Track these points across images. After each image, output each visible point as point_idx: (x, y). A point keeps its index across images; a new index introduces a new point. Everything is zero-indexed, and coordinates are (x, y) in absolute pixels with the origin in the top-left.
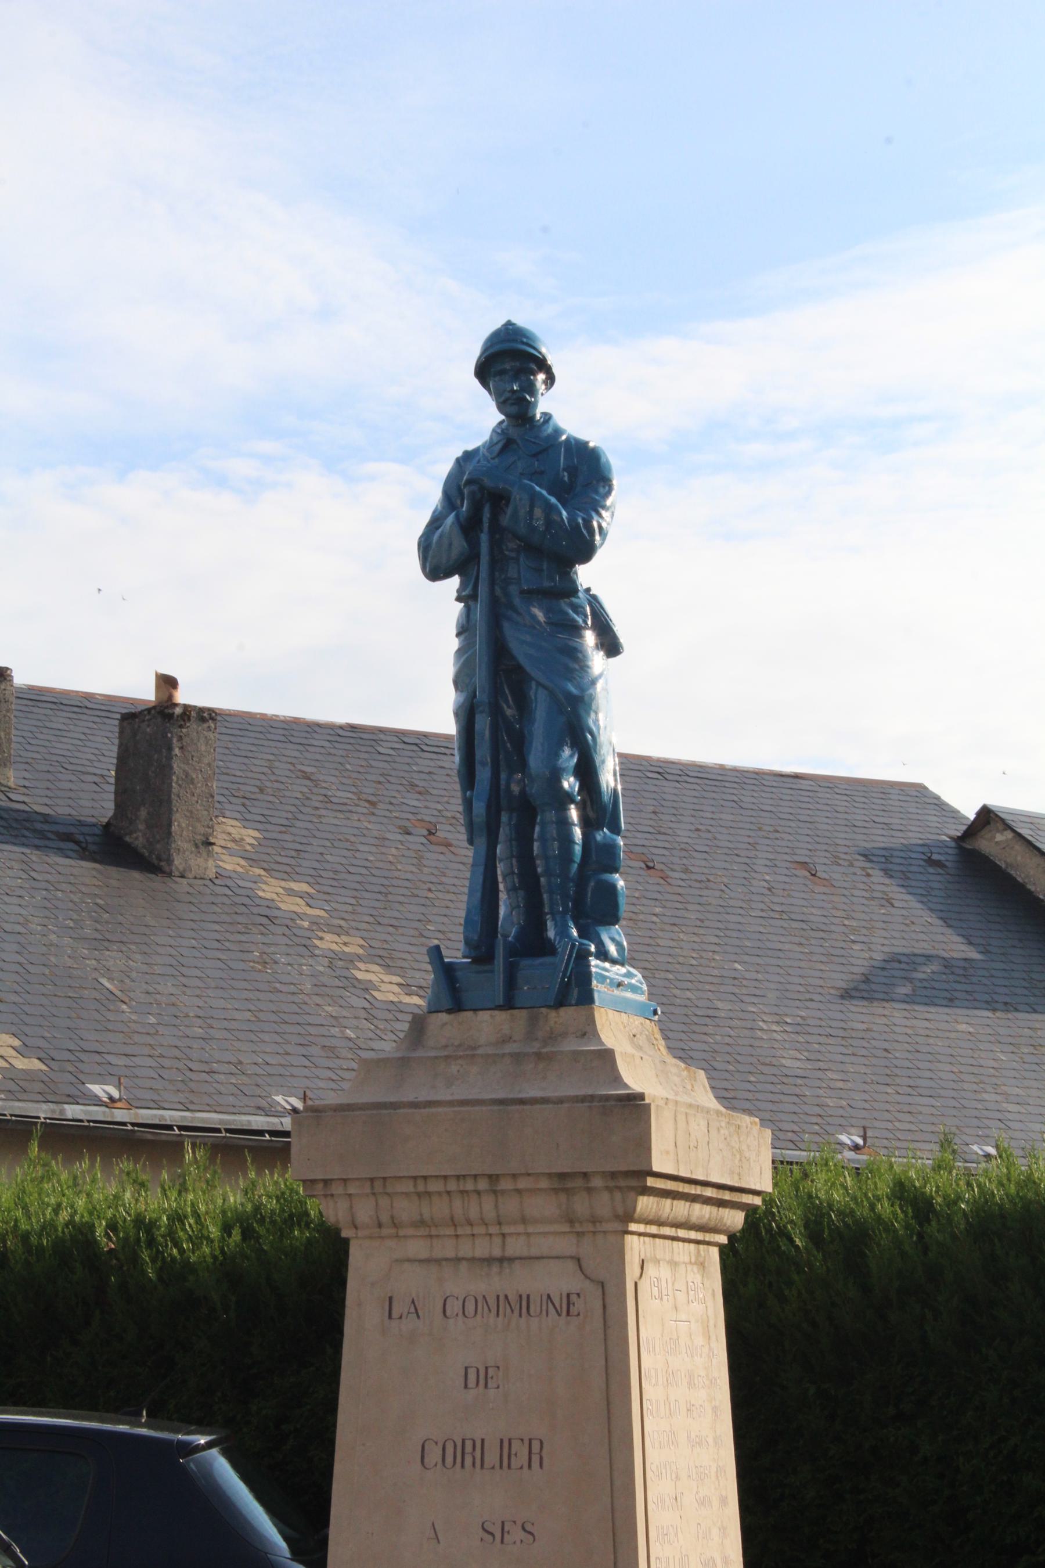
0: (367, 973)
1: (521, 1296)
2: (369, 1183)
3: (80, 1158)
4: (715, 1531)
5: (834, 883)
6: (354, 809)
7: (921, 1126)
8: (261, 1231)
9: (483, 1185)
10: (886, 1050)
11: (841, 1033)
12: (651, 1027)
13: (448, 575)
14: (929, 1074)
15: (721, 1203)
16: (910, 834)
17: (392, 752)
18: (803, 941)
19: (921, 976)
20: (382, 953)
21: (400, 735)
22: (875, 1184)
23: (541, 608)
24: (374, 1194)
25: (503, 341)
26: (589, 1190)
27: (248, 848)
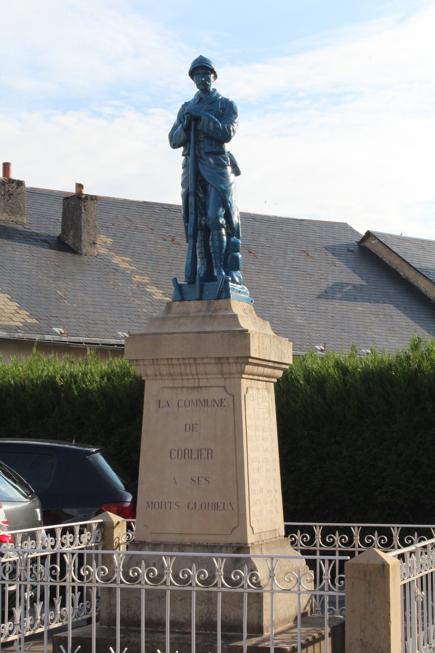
0: (151, 289)
1: (205, 400)
3: (50, 353)
4: (272, 480)
5: (315, 258)
6: (146, 231)
7: (345, 343)
8: (114, 378)
9: (192, 361)
10: (332, 316)
12: (250, 307)
13: (179, 147)
15: (275, 368)
16: (342, 241)
17: (159, 211)
18: (304, 278)
19: (345, 291)
20: (156, 282)
21: (162, 205)
22: (328, 362)
23: (212, 159)
25: (198, 63)
26: (229, 363)
27: (109, 245)
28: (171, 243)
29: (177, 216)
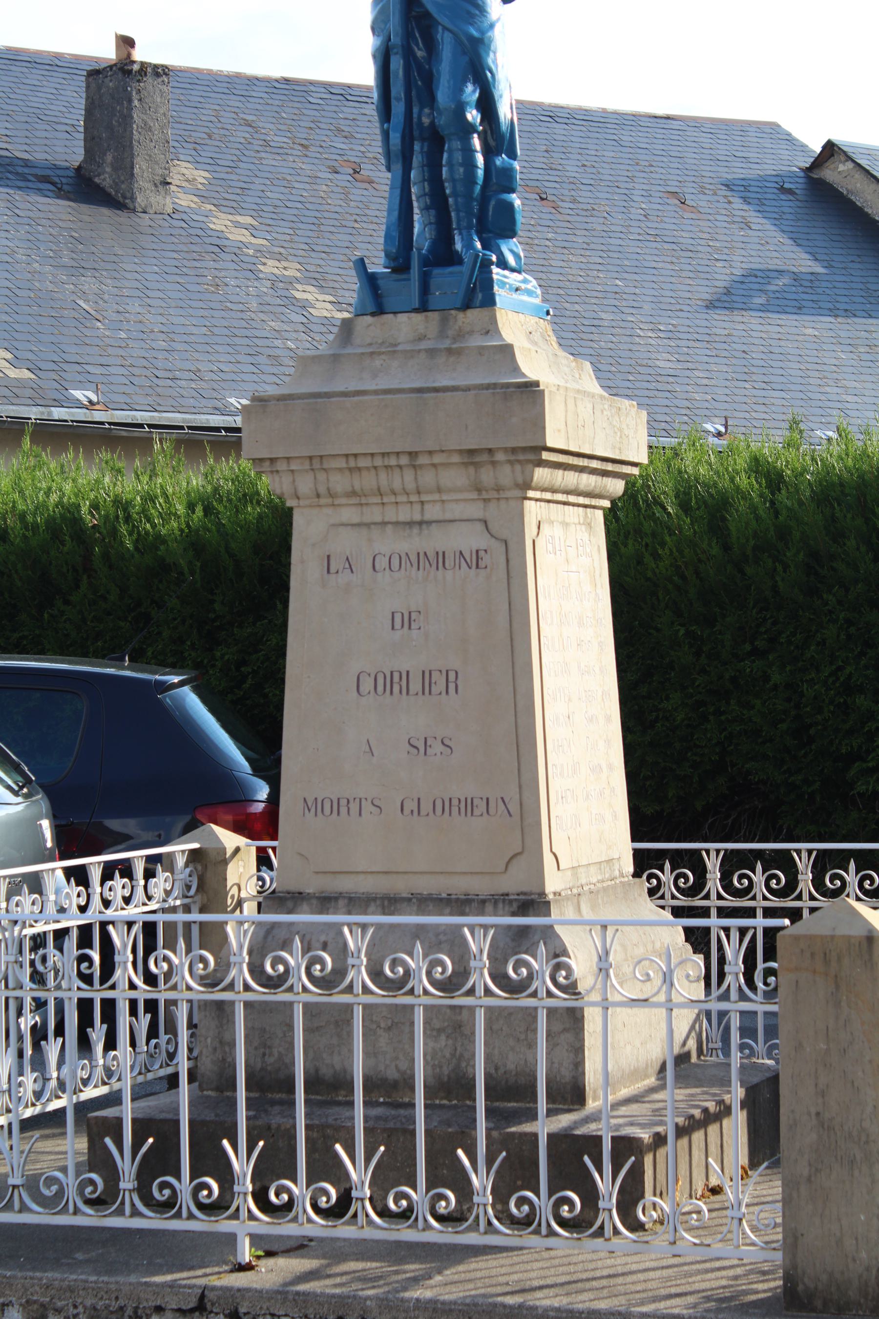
0: (305, 293)
2: (307, 462)
3: (66, 450)
6: (289, 152)
7: (774, 416)
8: (221, 508)
9: (404, 460)
11: (707, 338)
12: (544, 325)
14: (781, 372)
15: (605, 473)
16: (766, 167)
17: (321, 102)
20: (317, 276)
21: (328, 87)
24: (312, 470)
26: (494, 463)
27: (200, 186)
28: (351, 179)
29: (363, 111)
